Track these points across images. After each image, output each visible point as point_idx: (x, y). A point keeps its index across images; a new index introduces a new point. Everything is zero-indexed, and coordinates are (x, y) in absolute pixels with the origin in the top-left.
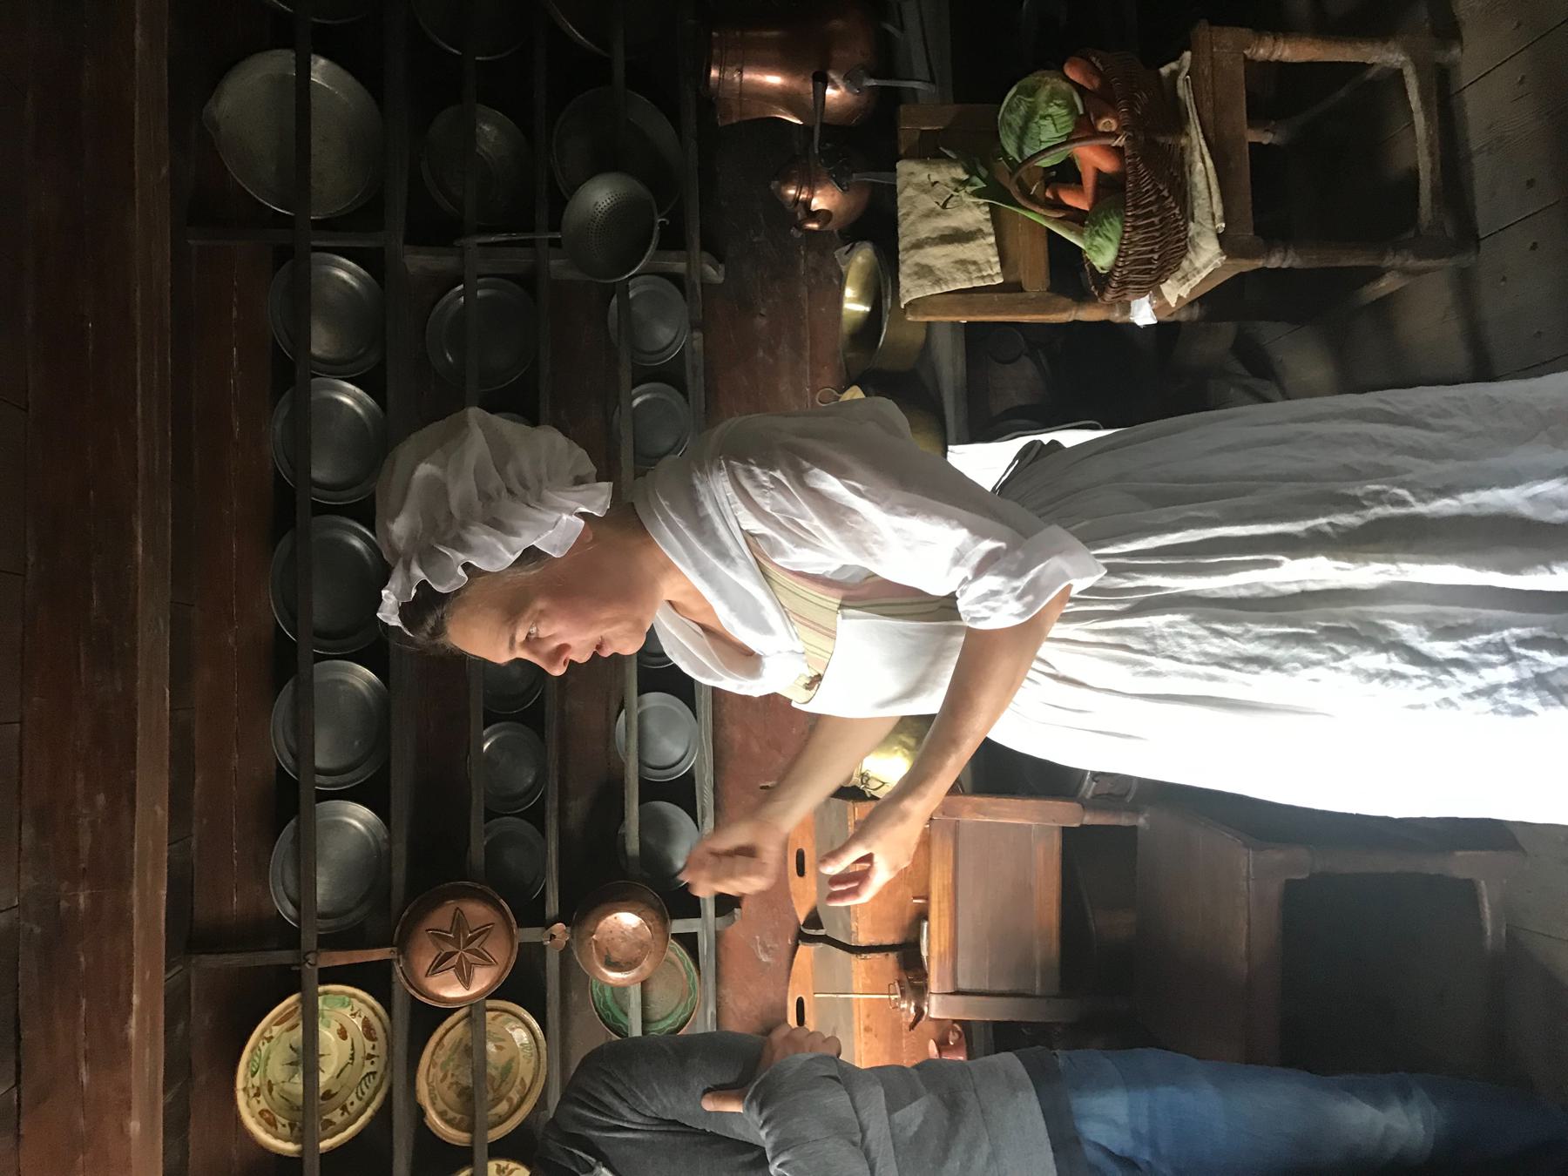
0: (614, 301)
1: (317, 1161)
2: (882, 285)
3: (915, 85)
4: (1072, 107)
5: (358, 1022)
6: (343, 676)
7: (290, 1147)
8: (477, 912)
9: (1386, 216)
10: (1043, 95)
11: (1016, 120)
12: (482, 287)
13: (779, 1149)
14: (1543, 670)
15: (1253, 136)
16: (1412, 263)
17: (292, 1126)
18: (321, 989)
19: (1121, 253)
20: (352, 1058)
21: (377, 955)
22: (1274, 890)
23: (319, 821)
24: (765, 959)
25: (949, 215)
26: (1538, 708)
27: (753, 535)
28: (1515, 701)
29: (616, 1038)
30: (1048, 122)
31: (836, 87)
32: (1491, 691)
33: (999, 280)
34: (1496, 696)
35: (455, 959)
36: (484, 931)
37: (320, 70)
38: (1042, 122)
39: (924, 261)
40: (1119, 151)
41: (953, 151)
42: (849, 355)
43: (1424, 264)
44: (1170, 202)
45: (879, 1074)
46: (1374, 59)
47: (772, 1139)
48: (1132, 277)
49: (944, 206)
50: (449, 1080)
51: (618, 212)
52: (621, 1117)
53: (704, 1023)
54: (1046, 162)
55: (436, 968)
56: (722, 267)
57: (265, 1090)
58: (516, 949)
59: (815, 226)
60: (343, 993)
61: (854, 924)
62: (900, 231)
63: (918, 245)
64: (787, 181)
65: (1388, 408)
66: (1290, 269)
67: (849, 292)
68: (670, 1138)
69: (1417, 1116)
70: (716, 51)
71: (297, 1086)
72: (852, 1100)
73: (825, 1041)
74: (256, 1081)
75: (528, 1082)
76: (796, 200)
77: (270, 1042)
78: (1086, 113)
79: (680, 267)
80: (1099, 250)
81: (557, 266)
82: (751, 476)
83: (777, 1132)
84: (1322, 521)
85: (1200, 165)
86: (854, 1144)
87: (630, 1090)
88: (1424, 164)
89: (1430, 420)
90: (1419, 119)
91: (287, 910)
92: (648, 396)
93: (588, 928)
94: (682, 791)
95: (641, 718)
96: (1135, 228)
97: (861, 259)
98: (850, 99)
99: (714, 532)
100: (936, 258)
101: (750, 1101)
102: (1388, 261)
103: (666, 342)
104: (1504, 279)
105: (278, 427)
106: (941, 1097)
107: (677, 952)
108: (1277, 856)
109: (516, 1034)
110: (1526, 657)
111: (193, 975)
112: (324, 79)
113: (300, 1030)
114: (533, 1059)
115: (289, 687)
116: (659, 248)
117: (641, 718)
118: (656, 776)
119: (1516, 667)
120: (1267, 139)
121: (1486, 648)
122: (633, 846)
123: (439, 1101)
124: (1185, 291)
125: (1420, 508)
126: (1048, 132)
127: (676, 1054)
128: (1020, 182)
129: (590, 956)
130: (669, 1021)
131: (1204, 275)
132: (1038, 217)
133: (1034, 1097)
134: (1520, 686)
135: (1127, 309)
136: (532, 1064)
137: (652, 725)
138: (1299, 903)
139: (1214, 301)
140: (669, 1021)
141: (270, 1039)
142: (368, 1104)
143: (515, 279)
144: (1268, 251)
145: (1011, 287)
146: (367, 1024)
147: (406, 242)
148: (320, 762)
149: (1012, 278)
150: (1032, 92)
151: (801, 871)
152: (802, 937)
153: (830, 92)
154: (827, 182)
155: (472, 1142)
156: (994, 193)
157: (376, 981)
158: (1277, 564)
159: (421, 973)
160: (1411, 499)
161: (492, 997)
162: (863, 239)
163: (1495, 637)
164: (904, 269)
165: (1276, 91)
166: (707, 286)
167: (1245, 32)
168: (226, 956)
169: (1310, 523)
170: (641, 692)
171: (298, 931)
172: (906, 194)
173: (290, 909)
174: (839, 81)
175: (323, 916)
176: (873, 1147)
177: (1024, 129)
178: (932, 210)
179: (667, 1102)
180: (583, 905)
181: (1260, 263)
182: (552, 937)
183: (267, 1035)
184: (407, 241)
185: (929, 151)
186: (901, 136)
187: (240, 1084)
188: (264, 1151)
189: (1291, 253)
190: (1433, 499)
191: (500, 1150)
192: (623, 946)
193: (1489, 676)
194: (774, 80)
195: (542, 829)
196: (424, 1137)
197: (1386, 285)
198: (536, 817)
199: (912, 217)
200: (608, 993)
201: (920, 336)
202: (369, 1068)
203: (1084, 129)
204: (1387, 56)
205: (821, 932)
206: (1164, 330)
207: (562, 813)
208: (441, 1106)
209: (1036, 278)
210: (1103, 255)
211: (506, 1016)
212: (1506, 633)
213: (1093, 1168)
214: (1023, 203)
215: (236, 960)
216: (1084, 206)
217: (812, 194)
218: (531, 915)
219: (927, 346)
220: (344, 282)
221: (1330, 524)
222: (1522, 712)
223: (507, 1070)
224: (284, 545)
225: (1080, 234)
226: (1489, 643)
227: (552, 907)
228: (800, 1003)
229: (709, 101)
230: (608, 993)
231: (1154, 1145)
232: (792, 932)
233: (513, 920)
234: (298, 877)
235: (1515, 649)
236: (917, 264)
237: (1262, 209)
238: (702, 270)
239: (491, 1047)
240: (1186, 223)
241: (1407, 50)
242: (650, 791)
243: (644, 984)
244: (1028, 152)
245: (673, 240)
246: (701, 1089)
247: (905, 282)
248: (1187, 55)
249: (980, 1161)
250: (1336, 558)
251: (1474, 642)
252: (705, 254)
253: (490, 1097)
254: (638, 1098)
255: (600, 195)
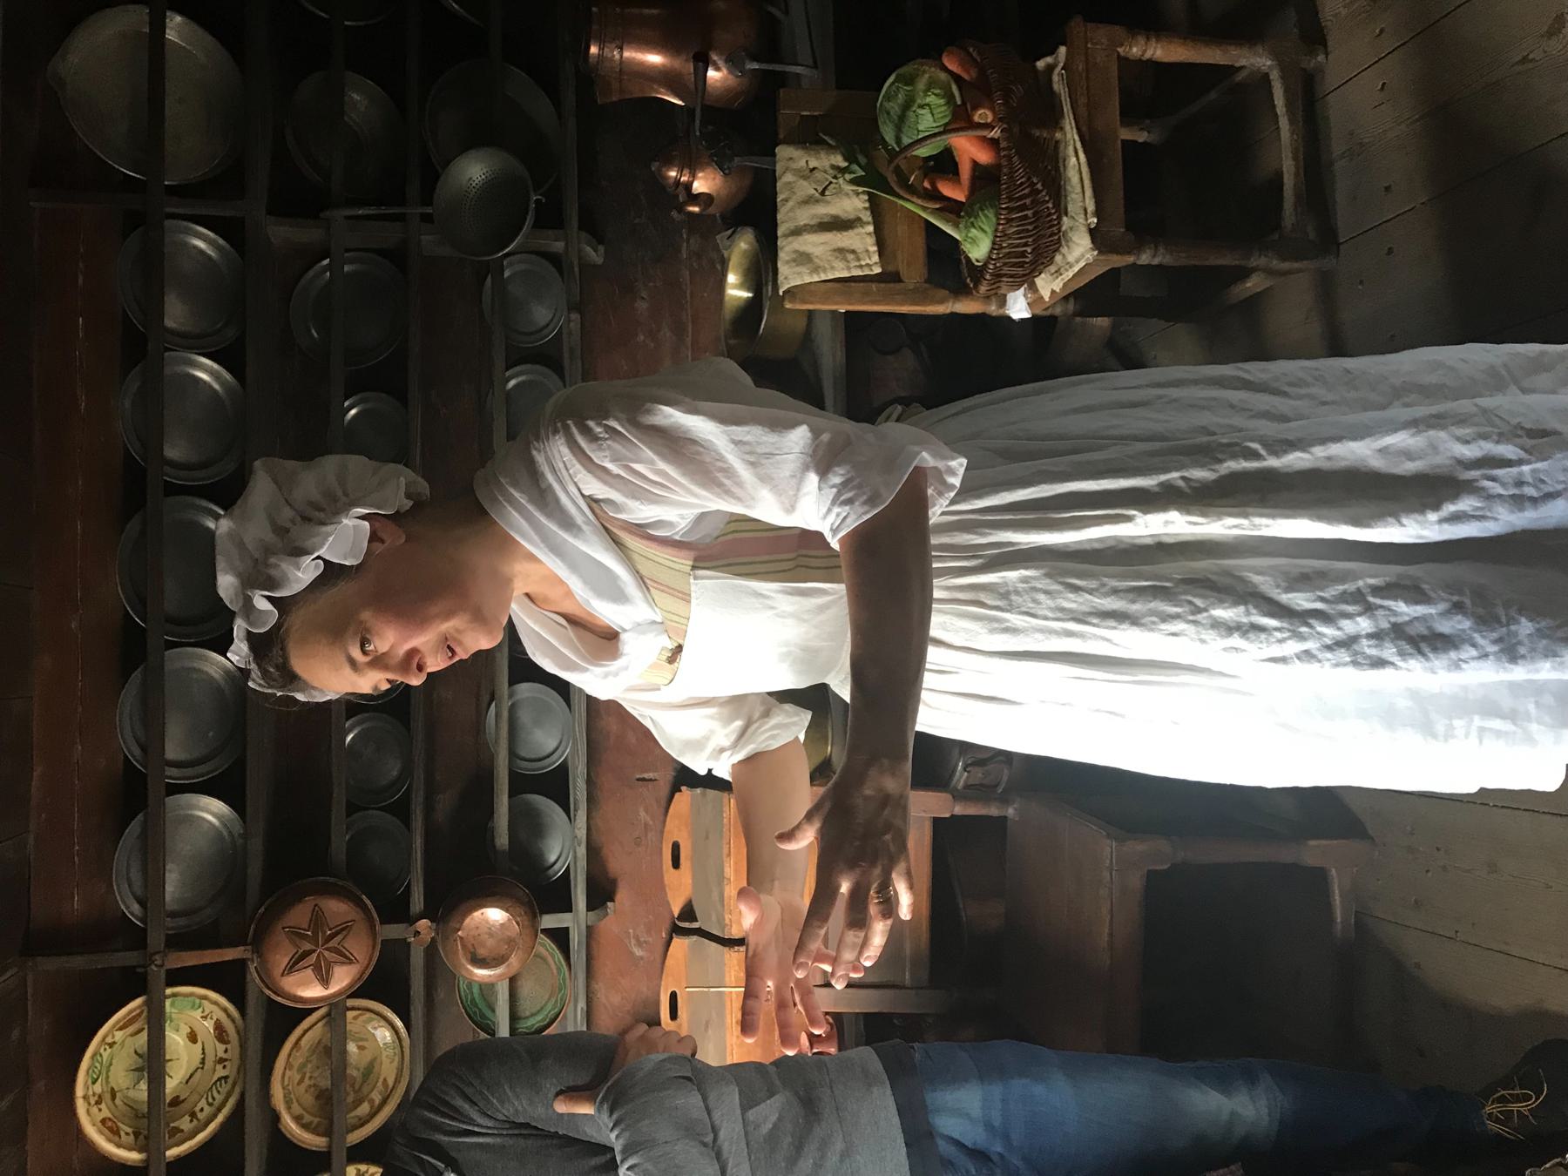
0: (489, 279)
1: (163, 1169)
2: (762, 271)
3: (798, 69)
4: (950, 98)
5: (209, 1025)
6: (188, 664)
7: (134, 1156)
8: (337, 909)
9: (1250, 216)
10: (921, 84)
11: (894, 107)
12: (351, 262)
13: (628, 1151)
14: (1400, 620)
15: (1126, 134)
16: (1276, 264)
17: (136, 1134)
18: (169, 991)
19: (995, 246)
20: (203, 1062)
21: (230, 954)
22: (1136, 881)
23: (169, 815)
24: (638, 952)
25: (828, 203)
26: (1396, 659)
27: (597, 501)
28: (1373, 652)
29: (483, 1035)
30: (925, 111)
31: (718, 69)
32: (1348, 643)
33: (877, 270)
34: (1355, 647)
35: (315, 956)
36: (344, 929)
37: (176, 27)
38: (921, 112)
39: (802, 249)
40: (994, 142)
41: (832, 136)
42: (732, 342)
43: (1286, 265)
44: (1044, 195)
45: (736, 1072)
46: (1243, 62)
47: (621, 1141)
48: (1006, 270)
49: (822, 194)
50: (307, 1082)
51: (492, 187)
52: (472, 1122)
53: (574, 1021)
54: (923, 151)
55: (292, 968)
56: (601, 248)
57: (108, 1096)
58: (379, 947)
59: (696, 209)
60: (191, 995)
61: (727, 917)
62: (779, 217)
63: (797, 232)
64: (669, 163)
65: (1246, 376)
66: (1160, 266)
67: (732, 278)
68: (522, 1141)
69: (1263, 1102)
70: (595, 27)
71: (142, 1092)
72: (705, 1099)
73: (681, 1040)
74: (98, 1088)
75: (391, 1083)
76: (677, 182)
77: (112, 1049)
78: (964, 103)
79: (559, 246)
80: (974, 241)
81: (429, 242)
82: (593, 438)
83: (627, 1134)
84: (1175, 475)
85: (1074, 160)
86: (705, 1145)
87: (481, 1093)
88: (1288, 167)
89: (1286, 389)
90: (1284, 123)
91: (133, 910)
92: (521, 379)
93: (453, 924)
94: (555, 784)
95: (512, 709)
96: (1009, 221)
97: (743, 245)
98: (732, 81)
99: (557, 500)
100: (814, 245)
101: (601, 1103)
102: (1254, 262)
103: (543, 323)
104: (1361, 282)
105: (127, 404)
106: (796, 1093)
107: (546, 946)
108: (1137, 847)
109: (379, 1035)
110: (1382, 607)
111: (30, 978)
112: (180, 37)
113: (145, 1034)
114: (397, 1059)
115: (137, 675)
116: (536, 226)
117: (512, 709)
118: (525, 768)
119: (1372, 617)
120: (1142, 137)
121: (1344, 598)
122: (502, 840)
123: (295, 1105)
124: (1057, 286)
125: (1273, 462)
126: (927, 121)
127: (535, 1053)
128: (898, 171)
129: (456, 952)
130: (539, 1018)
131: (1076, 269)
132: (913, 206)
133: (889, 1092)
134: (1377, 636)
135: (1003, 302)
136: (396, 1063)
137: (525, 716)
138: (1165, 897)
139: (1090, 295)
140: (539, 1018)
141: (111, 1045)
142: (219, 1110)
143: (380, 252)
144: (1137, 248)
145: (889, 277)
146: (219, 1027)
147: (269, 213)
148: (172, 752)
149: (890, 268)
150: (910, 80)
151: (676, 864)
152: (676, 930)
153: (712, 74)
154: (708, 164)
155: (330, 1146)
156: (873, 182)
157: (228, 981)
158: (1129, 519)
159: (277, 972)
160: (1263, 452)
161: (354, 995)
162: (746, 224)
163: (1350, 587)
164: (783, 256)
165: (1149, 91)
166: (585, 266)
167: (1119, 31)
168: (64, 958)
169: (1163, 478)
170: (512, 683)
171: (145, 930)
172: (785, 179)
173: (136, 907)
174: (721, 63)
175: (173, 915)
176: (726, 1147)
177: (902, 118)
178: (811, 197)
179: (519, 1105)
180: (448, 903)
181: (1131, 259)
182: (417, 933)
183: (109, 1040)
184: (269, 213)
185: (809, 138)
186: (780, 118)
187: (80, 1091)
188: (106, 1159)
189: (1161, 250)
190: (1285, 452)
191: (359, 1154)
192: (490, 942)
193: (1349, 627)
194: (655, 59)
195: (406, 821)
196: (279, 1142)
197: (1254, 284)
198: (401, 810)
199: (791, 204)
200: (476, 990)
201: (801, 324)
202: (221, 1072)
203: (961, 120)
204: (1255, 60)
205: (695, 925)
206: (1040, 324)
207: (429, 809)
208: (297, 1109)
209: (914, 271)
210: (978, 247)
211: (368, 1015)
212: (1360, 583)
213: (948, 1163)
214: (901, 193)
215: (78, 962)
216: (959, 195)
217: (694, 177)
218: (396, 911)
219: (808, 337)
220: (201, 252)
221: (1183, 478)
222: (1380, 663)
223: (369, 1070)
224: (134, 526)
225: (956, 226)
226: (1345, 592)
227: (417, 902)
228: (673, 996)
229: (589, 77)
230: (476, 990)
231: (1006, 1137)
232: (666, 926)
233: (375, 916)
234: (145, 872)
235: (1371, 599)
236: (796, 251)
237: (1133, 210)
238: (580, 251)
239: (352, 1047)
240: (1059, 218)
241: (1275, 55)
242: (521, 784)
243: (513, 981)
244: (906, 141)
245: (550, 219)
246: (554, 1091)
247: (783, 269)
248: (1063, 50)
249: (833, 1159)
250: (1189, 513)
251: (1330, 593)
252: (584, 234)
253: (350, 1099)
254: (487, 1100)
255: (474, 171)
